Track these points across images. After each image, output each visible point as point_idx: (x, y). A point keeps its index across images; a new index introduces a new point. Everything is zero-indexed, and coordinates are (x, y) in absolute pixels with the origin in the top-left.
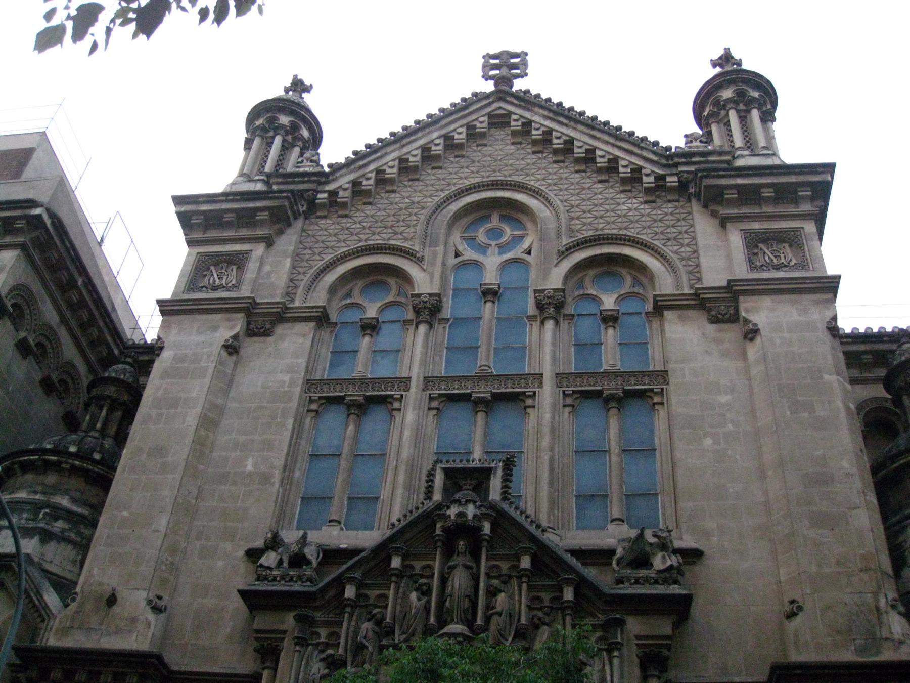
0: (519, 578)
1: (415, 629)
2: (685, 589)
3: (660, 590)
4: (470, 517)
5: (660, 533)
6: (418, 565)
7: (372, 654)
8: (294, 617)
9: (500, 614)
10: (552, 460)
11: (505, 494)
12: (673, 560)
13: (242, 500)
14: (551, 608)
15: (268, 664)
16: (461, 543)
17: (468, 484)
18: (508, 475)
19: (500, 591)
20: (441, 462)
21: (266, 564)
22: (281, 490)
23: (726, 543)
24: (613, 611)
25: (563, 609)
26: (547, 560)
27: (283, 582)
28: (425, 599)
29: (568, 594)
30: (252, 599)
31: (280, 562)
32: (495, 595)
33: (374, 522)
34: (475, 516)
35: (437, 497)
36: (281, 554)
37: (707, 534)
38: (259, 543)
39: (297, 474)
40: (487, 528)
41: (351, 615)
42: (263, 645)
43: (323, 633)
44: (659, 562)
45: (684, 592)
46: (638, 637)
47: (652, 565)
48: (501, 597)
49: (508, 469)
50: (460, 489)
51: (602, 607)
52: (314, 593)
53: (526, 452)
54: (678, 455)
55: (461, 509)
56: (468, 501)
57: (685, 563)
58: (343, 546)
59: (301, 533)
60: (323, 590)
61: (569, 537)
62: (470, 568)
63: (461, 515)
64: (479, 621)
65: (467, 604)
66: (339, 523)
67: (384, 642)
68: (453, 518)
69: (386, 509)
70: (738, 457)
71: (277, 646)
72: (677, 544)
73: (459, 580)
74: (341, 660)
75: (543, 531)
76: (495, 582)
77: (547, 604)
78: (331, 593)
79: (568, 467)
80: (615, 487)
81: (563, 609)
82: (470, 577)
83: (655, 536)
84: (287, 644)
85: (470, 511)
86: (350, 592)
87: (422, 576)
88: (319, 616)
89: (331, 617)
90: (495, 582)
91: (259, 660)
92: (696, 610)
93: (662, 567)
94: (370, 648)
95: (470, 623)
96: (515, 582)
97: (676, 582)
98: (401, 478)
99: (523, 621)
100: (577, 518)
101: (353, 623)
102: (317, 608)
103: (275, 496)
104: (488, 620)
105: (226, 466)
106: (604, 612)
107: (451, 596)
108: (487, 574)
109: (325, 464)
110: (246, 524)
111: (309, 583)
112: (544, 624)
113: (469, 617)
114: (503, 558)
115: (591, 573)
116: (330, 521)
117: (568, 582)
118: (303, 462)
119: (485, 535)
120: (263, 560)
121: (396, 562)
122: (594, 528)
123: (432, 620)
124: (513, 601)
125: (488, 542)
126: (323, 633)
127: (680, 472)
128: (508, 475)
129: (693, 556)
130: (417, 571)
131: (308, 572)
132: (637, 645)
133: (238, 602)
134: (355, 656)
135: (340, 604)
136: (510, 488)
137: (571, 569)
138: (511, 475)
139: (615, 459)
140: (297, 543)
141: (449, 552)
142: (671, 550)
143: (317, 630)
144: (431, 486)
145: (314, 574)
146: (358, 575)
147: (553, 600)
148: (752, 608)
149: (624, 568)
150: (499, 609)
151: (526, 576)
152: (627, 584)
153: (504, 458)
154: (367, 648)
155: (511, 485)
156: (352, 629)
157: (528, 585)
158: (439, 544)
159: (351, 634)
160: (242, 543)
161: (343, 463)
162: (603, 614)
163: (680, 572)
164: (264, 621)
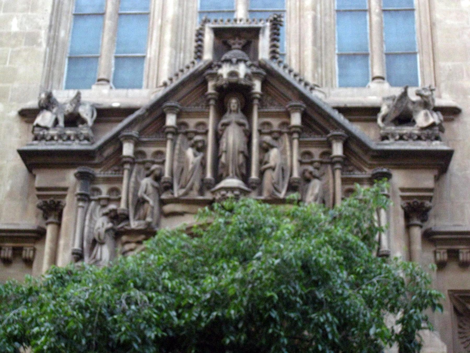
0: (290, 134)
1: (193, 184)
2: (444, 145)
3: (423, 146)
6: (192, 123)
7: (153, 208)
8: (75, 175)
9: (273, 169)
10: (315, 18)
11: (274, 54)
12: (435, 118)
13: (10, 62)
14: (321, 163)
15: (51, 219)
17: (236, 43)
19: (272, 147)
20: (209, 21)
21: (42, 124)
22: (48, 50)
24: (380, 165)
25: (333, 164)
26: (315, 116)
27: (60, 141)
30: (33, 160)
31: (56, 122)
33: (142, 80)
34: (246, 75)
35: (208, 56)
36: (56, 114)
38: (33, 103)
39: (62, 34)
40: (257, 87)
41: (131, 172)
42: (46, 202)
43: (104, 189)
44: (422, 119)
45: (445, 148)
46: (403, 190)
47: (414, 122)
48: (274, 153)
50: (229, 48)
51: (370, 162)
53: (288, 10)
54: (438, 16)
55: (232, 68)
56: (239, 61)
57: (446, 120)
58: (116, 105)
61: (333, 95)
63: (233, 74)
64: (254, 176)
65: (241, 159)
66: (108, 81)
67: (164, 196)
69: (154, 67)
71: (59, 202)
72: (439, 102)
73: (233, 138)
74: (123, 214)
75: (312, 89)
76: (268, 138)
77: (317, 158)
78: (108, 151)
79: (330, 26)
80: (376, 45)
81: (333, 164)
82: (243, 134)
83: (418, 94)
84: (69, 202)
86: (128, 150)
87: (196, 133)
88: (98, 173)
89: (109, 174)
90: (268, 138)
91: (41, 216)
92: (454, 165)
93: (425, 124)
94: (151, 202)
95: (245, 178)
96: (286, 138)
97: (437, 138)
98: (168, 37)
99: (296, 175)
100: (340, 76)
101: (133, 179)
103: (43, 55)
104: (261, 174)
106: (371, 166)
107: (226, 152)
109: (90, 23)
110: (16, 85)
111: (86, 142)
112: (315, 177)
113: (244, 171)
115: (356, 128)
116: (99, 80)
117: (337, 138)
118: (67, 22)
119: (257, 93)
120: (39, 120)
121: (171, 120)
122: (354, 86)
123: (209, 175)
124: (285, 156)
125: (260, 100)
126: (104, 189)
127: (438, 33)
128: (275, 34)
129: (451, 113)
131: (84, 130)
133: (18, 162)
134: (136, 210)
135: (118, 161)
137: (339, 126)
138: (278, 35)
139: (375, 19)
140: (71, 102)
141: (222, 110)
142: (432, 108)
144: (200, 46)
145: (91, 134)
146: (134, 132)
147: (323, 154)
149: (387, 125)
150: (272, 163)
152: (392, 140)
153: (271, 18)
154: (147, 201)
155: (278, 44)
156: (132, 184)
158: (212, 102)
160: (14, 103)
161: (109, 23)
162: (370, 168)
163: (442, 130)
164: (44, 179)
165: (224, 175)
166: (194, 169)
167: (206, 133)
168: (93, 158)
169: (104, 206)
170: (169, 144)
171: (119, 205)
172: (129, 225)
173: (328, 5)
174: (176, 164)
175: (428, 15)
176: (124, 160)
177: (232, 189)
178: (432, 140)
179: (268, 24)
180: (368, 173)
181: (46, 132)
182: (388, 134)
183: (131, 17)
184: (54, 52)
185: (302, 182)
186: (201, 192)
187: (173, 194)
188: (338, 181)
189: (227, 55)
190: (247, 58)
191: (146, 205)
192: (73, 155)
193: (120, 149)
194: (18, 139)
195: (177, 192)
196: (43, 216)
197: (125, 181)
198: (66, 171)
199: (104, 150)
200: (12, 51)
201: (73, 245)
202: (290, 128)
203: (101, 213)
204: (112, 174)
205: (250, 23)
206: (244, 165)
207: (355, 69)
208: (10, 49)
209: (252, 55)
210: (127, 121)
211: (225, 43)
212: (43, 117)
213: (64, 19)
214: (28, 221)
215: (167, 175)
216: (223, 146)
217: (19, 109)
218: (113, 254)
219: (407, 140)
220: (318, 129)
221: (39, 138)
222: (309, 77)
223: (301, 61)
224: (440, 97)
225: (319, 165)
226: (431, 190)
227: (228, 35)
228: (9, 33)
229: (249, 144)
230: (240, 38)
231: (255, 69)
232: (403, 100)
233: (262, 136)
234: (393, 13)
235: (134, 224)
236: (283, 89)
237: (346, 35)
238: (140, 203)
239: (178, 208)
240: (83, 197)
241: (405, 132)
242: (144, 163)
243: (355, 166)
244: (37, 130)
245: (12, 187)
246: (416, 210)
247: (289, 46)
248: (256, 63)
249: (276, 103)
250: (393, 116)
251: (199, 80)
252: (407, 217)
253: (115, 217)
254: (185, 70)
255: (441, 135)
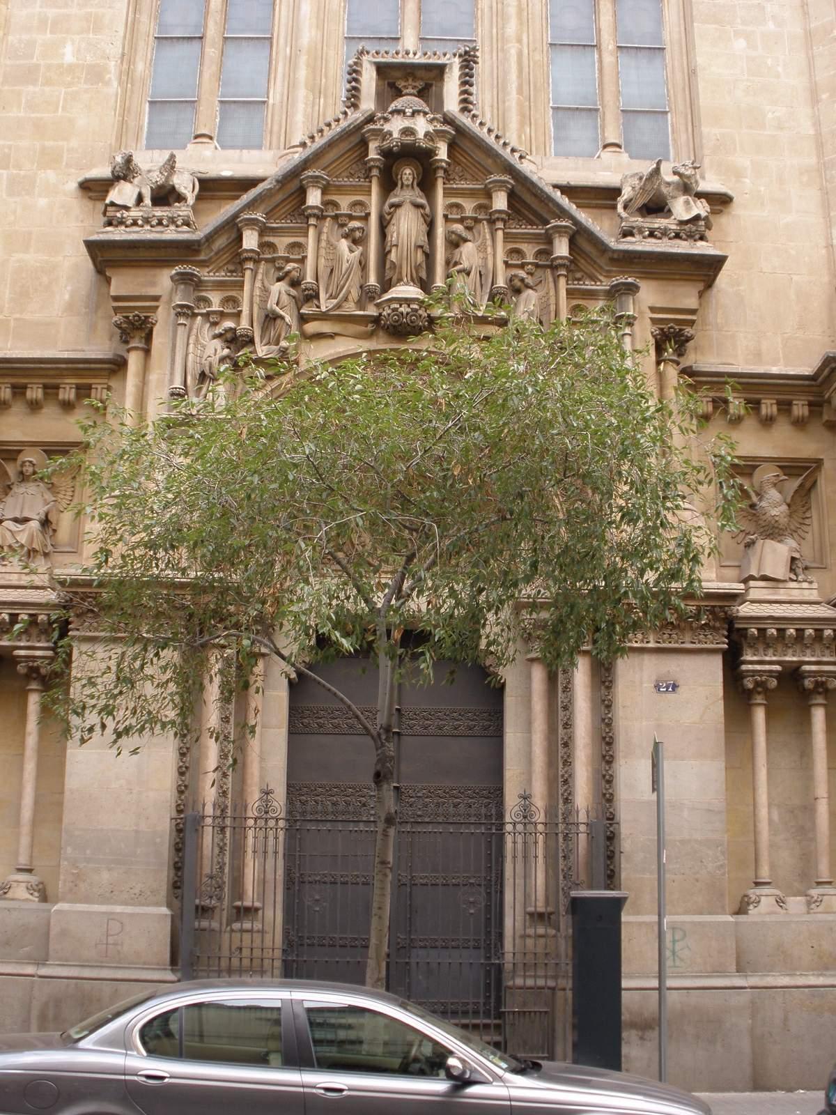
0: (492, 222)
1: (349, 292)
2: (715, 247)
4: (421, 135)
5: (682, 170)
6: (344, 202)
8: (172, 278)
10: (520, 54)
11: (466, 105)
12: (701, 208)
13: (64, 109)
14: (537, 266)
15: (135, 343)
16: (408, 171)
18: (467, 75)
19: (466, 240)
21: (118, 202)
23: (762, 189)
24: (623, 273)
28: (359, 250)
29: (562, 248)
30: (106, 257)
31: (140, 199)
32: (457, 246)
34: (427, 134)
37: (738, 174)
38: (103, 171)
39: (140, 66)
40: (442, 153)
42: (127, 317)
43: (215, 299)
44: (682, 208)
46: (653, 309)
49: (467, 67)
50: (399, 93)
52: (198, 242)
54: (700, 60)
55: (407, 123)
56: (414, 113)
58: (227, 173)
59: (166, 155)
60: (210, 238)
61: (549, 169)
62: (418, 206)
64: (439, 282)
65: (420, 257)
68: (396, 135)
70: (780, 69)
71: (147, 317)
73: (407, 226)
76: (458, 228)
77: (530, 258)
78: (221, 242)
81: (554, 268)
83: (675, 173)
84: (162, 319)
85: (422, 126)
86: (250, 240)
87: (351, 218)
88: (205, 274)
89: (221, 276)
90: (458, 228)
92: (723, 279)
93: (686, 217)
94: (288, 319)
95: (425, 285)
96: (485, 228)
97: (702, 238)
98: (302, 73)
99: (501, 283)
100: (557, 139)
101: (258, 284)
102: (203, 264)
103: (113, 101)
105: (32, 58)
107: (397, 246)
108: (445, 216)
110: (74, 143)
111: (185, 228)
112: (528, 287)
113: (424, 275)
114: (471, 193)
116: (197, 137)
118: (145, 48)
119: (442, 160)
120: (114, 196)
121: (314, 198)
123: (372, 280)
124: (485, 254)
125: (446, 171)
126: (215, 299)
128: (467, 75)
129: (720, 201)
130: (344, 209)
132: (651, 319)
134: (264, 330)
135: (237, 259)
136: (471, 94)
137: (563, 213)
141: (389, 184)
143: (204, 294)
147: (539, 253)
148: (795, 278)
149: (631, 214)
150: (465, 265)
151: (502, 219)
152: (638, 238)
153: (462, 51)
154: (283, 318)
157: (504, 233)
158: (375, 172)
159: (257, 300)
161: (211, 52)
163: (708, 227)
165: (395, 279)
166: (349, 270)
167: (366, 217)
168: (197, 252)
169: (215, 324)
170: (311, 231)
171: (238, 323)
172: (255, 352)
173: (538, 36)
174: (322, 261)
175: (685, 58)
176: (245, 255)
177: (408, 301)
178: (695, 241)
179: (457, 60)
180: (604, 284)
181: (126, 214)
182: (634, 228)
183: (244, 43)
184: (128, 93)
185: (509, 293)
186: (360, 304)
187: (318, 307)
188: (563, 294)
189: (398, 104)
190: (427, 109)
191: (278, 321)
192: (155, 253)
193: (240, 238)
194: (79, 224)
195: (325, 304)
196: (121, 337)
197: (247, 287)
198: (157, 271)
199: (213, 242)
200: (66, 93)
201: (171, 381)
202: (491, 214)
203: (211, 334)
204: (226, 276)
205: (430, 58)
206: (424, 265)
207: (579, 131)
208: (63, 90)
209: (433, 101)
210: (253, 193)
211: (392, 86)
212: (120, 192)
213: (141, 44)
214: (99, 348)
215: (309, 279)
216: (392, 237)
217: (80, 179)
218: (232, 392)
219: (660, 238)
220: (531, 216)
221: (115, 223)
222: (512, 138)
223: (502, 117)
224: (703, 178)
225: (533, 268)
226: (693, 312)
227: (397, 74)
228: (60, 66)
229: (431, 233)
230: (415, 78)
231: (439, 127)
232: (654, 179)
233: (449, 224)
234: (633, 51)
235: (262, 351)
236: (479, 156)
237: (568, 79)
238: (271, 319)
239: (326, 327)
240: (185, 310)
241: (656, 226)
242: (273, 260)
243: (586, 273)
244: (111, 212)
245: (72, 297)
246: (672, 338)
247: (483, 94)
248: (438, 116)
249: (468, 176)
250: (640, 202)
251: (355, 139)
252: (659, 349)
253: (235, 340)
254: (333, 124)
255: (708, 233)
